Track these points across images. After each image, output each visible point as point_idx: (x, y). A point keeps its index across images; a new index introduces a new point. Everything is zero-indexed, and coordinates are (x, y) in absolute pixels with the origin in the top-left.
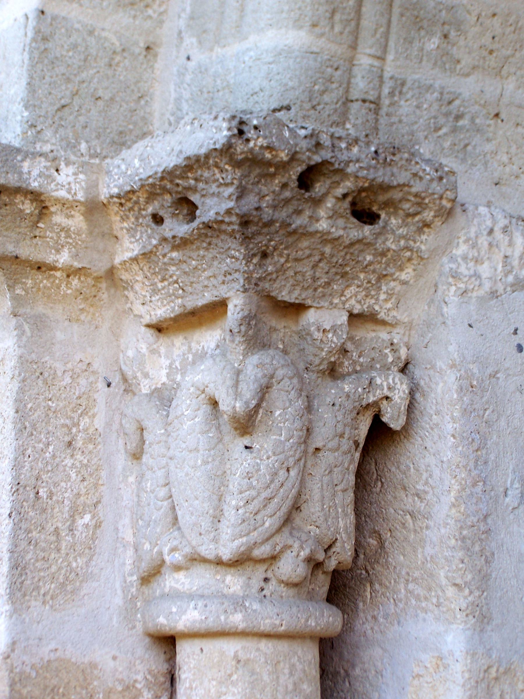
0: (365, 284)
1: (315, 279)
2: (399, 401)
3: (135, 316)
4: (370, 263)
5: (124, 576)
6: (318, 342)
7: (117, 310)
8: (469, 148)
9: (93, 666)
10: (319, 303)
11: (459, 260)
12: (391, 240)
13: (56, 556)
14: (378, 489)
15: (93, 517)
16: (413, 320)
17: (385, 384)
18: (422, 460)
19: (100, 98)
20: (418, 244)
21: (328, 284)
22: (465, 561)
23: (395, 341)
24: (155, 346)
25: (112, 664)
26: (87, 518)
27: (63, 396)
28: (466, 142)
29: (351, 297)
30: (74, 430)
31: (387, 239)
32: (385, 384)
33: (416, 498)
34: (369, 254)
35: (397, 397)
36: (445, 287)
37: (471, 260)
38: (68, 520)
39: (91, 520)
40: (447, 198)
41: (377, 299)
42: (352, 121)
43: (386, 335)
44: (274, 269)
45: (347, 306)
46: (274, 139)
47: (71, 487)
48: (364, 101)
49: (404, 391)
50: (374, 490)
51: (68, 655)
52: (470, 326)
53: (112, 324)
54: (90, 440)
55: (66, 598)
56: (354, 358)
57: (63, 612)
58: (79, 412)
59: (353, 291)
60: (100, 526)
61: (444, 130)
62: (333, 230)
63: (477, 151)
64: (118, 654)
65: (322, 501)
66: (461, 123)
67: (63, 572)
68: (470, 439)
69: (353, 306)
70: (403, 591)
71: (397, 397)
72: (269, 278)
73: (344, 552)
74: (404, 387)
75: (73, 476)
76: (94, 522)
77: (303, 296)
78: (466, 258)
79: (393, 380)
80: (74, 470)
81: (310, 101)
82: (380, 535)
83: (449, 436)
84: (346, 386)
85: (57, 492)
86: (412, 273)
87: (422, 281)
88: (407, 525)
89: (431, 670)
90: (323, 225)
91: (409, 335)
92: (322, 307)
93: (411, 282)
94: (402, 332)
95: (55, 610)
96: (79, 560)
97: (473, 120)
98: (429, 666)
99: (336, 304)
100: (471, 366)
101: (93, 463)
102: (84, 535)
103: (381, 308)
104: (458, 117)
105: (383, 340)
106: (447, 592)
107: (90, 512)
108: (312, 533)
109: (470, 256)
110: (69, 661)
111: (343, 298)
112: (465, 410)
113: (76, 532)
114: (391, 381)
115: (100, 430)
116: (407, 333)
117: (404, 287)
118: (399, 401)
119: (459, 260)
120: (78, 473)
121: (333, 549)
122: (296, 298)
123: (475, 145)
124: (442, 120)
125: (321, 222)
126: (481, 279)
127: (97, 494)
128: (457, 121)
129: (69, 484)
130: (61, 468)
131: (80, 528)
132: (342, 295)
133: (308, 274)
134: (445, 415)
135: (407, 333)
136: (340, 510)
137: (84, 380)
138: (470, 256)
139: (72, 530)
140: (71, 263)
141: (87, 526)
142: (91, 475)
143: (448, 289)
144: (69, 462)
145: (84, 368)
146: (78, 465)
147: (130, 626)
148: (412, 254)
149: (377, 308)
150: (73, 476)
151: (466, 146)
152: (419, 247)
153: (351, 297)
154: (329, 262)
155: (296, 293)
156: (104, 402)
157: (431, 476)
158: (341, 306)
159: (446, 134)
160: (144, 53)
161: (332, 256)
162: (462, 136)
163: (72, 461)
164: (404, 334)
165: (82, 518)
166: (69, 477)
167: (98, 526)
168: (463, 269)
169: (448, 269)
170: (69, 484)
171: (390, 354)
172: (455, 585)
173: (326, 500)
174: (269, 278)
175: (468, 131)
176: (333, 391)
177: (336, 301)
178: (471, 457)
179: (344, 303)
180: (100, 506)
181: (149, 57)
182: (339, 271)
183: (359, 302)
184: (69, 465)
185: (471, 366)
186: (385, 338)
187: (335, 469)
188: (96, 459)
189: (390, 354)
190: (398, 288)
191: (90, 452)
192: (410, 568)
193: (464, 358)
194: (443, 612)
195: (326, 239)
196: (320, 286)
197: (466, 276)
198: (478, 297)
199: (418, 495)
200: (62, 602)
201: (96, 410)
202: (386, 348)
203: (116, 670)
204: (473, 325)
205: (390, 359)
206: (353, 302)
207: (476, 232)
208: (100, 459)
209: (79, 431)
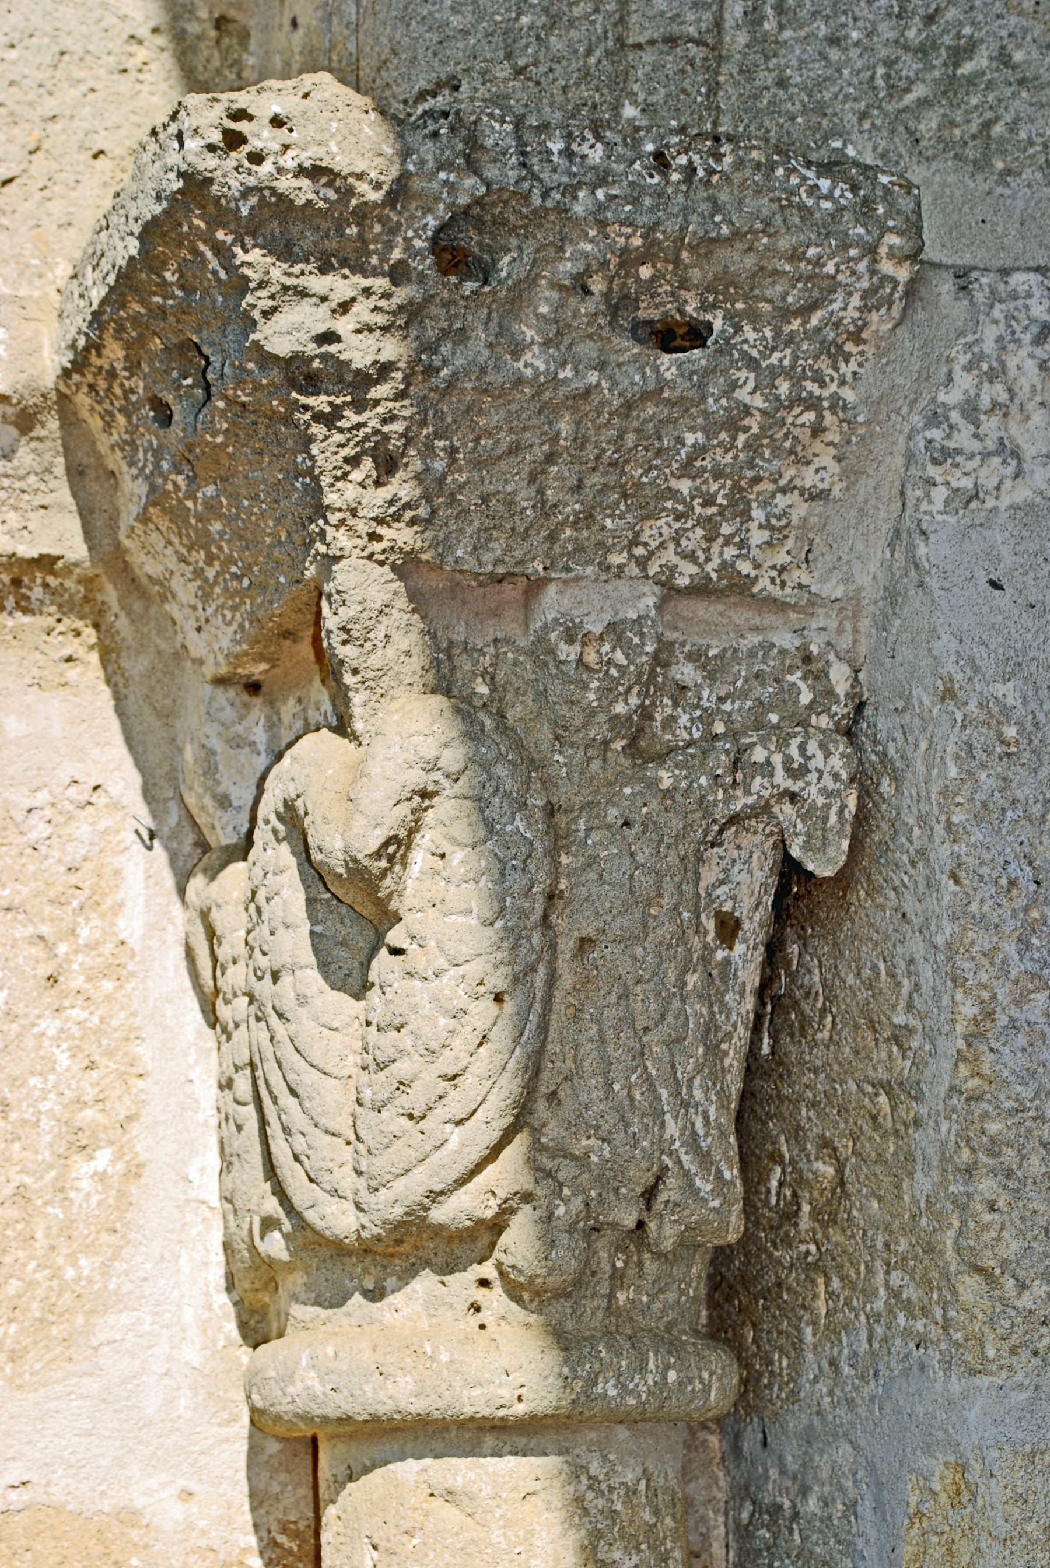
0: (698, 510)
1: (545, 509)
2: (821, 801)
3: (194, 661)
4: (699, 451)
5: (207, 1294)
6: (570, 670)
7: (159, 652)
8: (998, 129)
9: (130, 1517)
10: (568, 569)
11: (955, 416)
12: (751, 384)
13: (21, 1254)
14: (826, 1034)
15: (118, 1156)
16: (858, 590)
17: (777, 759)
18: (899, 949)
19: (102, 152)
20: (833, 387)
21: (587, 518)
22: (1001, 1204)
23: (814, 649)
24: (239, 729)
25: (177, 1511)
26: (103, 1158)
27: (31, 868)
28: (989, 115)
29: (662, 546)
30: (63, 948)
31: (734, 385)
32: (777, 759)
33: (895, 1049)
34: (692, 429)
35: (814, 790)
36: (919, 493)
37: (989, 412)
38: (51, 1166)
39: (113, 1162)
40: (891, 256)
41: (742, 545)
42: (641, 97)
43: (789, 636)
44: (418, 492)
45: (653, 569)
46: (334, 148)
47: (56, 1085)
48: (672, 41)
49: (836, 776)
50: (819, 1036)
51: (57, 1494)
52: (995, 585)
53: (152, 689)
54: (114, 970)
55: (49, 1357)
56: (705, 703)
57: (42, 1392)
58: (75, 903)
59: (665, 531)
60: (138, 1176)
61: (919, 91)
62: (567, 373)
63: (1023, 135)
64: (193, 1487)
65: (605, 1074)
66: (967, 68)
67: (40, 1292)
68: (1004, 882)
69: (673, 569)
70: (882, 1291)
71: (814, 790)
72: (408, 515)
73: (709, 1200)
74: (836, 762)
75: (63, 1059)
76: (120, 1167)
77: (518, 554)
78: (976, 409)
79: (802, 748)
80: (64, 1046)
81: (509, 56)
82: (835, 1149)
83: (945, 878)
84: (663, 774)
85: (20, 1101)
86: (834, 467)
87: (865, 487)
88: (880, 1120)
89: (943, 1498)
90: (534, 362)
91: (856, 631)
92: (578, 579)
93: (836, 492)
94: (834, 625)
95: (19, 1387)
96: (83, 1262)
97: (1004, 59)
98: (937, 1487)
99: (621, 567)
100: (1000, 689)
101: (115, 1023)
102: (95, 1199)
103: (757, 566)
104: (960, 53)
105: (783, 652)
106: (961, 1289)
107: (111, 1143)
108: (594, 1158)
109: (985, 402)
110: (59, 1509)
111: (639, 551)
112: (985, 805)
113: (72, 1195)
114: (794, 751)
115: (134, 942)
116: (848, 625)
117: (818, 506)
118: (821, 801)
119: (955, 416)
120: (75, 1051)
121: (662, 1197)
122: (496, 562)
123: (1016, 121)
124: (909, 66)
125: (528, 357)
126: (1020, 460)
127: (127, 1101)
128: (957, 65)
129: (52, 1078)
130: (30, 1042)
131: (85, 1185)
132: (635, 542)
133: (523, 494)
134: (934, 823)
135: (848, 625)
136: (664, 1093)
137: (85, 828)
138: (985, 402)
139: (62, 1190)
140: (10, 550)
141: (101, 1177)
142: (110, 1054)
143: (928, 495)
144: (50, 1026)
145: (85, 797)
146: (75, 1031)
147: (225, 1415)
148: (820, 417)
149: (745, 567)
150: (63, 1059)
151: (987, 125)
152: (835, 398)
153: (662, 546)
154: (574, 460)
155: (498, 548)
156: (141, 876)
157: (917, 987)
158: (636, 571)
159: (924, 103)
160: (213, 34)
161: (580, 441)
162: (974, 101)
163: (58, 1023)
164: (840, 631)
165: (92, 1158)
166: (51, 1064)
167: (135, 1172)
168: (964, 439)
169: (922, 444)
170: (52, 1078)
171: (802, 685)
172: (980, 1270)
173: (617, 1072)
174: (408, 515)
175: (990, 86)
176: (627, 791)
177: (617, 559)
178: (1009, 926)
179: (643, 563)
180: (135, 1129)
181: (226, 41)
182: (612, 479)
183: (691, 557)
184: (52, 1032)
185: (1000, 689)
186: (787, 645)
187: (639, 989)
188: (122, 1015)
189: (802, 685)
190: (801, 509)
191: (109, 998)
192: (892, 1232)
193: (977, 670)
194: (958, 1345)
195: (546, 398)
196: (563, 524)
197: (971, 457)
198: (1014, 507)
199: (896, 1039)
200: (38, 1366)
201: (120, 896)
202: (791, 670)
203: (191, 1527)
204: (1004, 582)
205: (806, 698)
206: (669, 556)
207: (999, 339)
208: (134, 1014)
209: (77, 952)
